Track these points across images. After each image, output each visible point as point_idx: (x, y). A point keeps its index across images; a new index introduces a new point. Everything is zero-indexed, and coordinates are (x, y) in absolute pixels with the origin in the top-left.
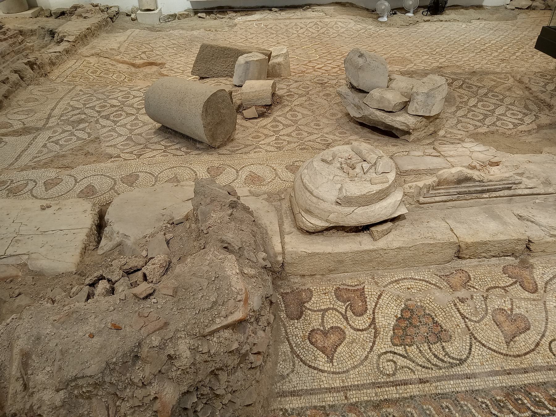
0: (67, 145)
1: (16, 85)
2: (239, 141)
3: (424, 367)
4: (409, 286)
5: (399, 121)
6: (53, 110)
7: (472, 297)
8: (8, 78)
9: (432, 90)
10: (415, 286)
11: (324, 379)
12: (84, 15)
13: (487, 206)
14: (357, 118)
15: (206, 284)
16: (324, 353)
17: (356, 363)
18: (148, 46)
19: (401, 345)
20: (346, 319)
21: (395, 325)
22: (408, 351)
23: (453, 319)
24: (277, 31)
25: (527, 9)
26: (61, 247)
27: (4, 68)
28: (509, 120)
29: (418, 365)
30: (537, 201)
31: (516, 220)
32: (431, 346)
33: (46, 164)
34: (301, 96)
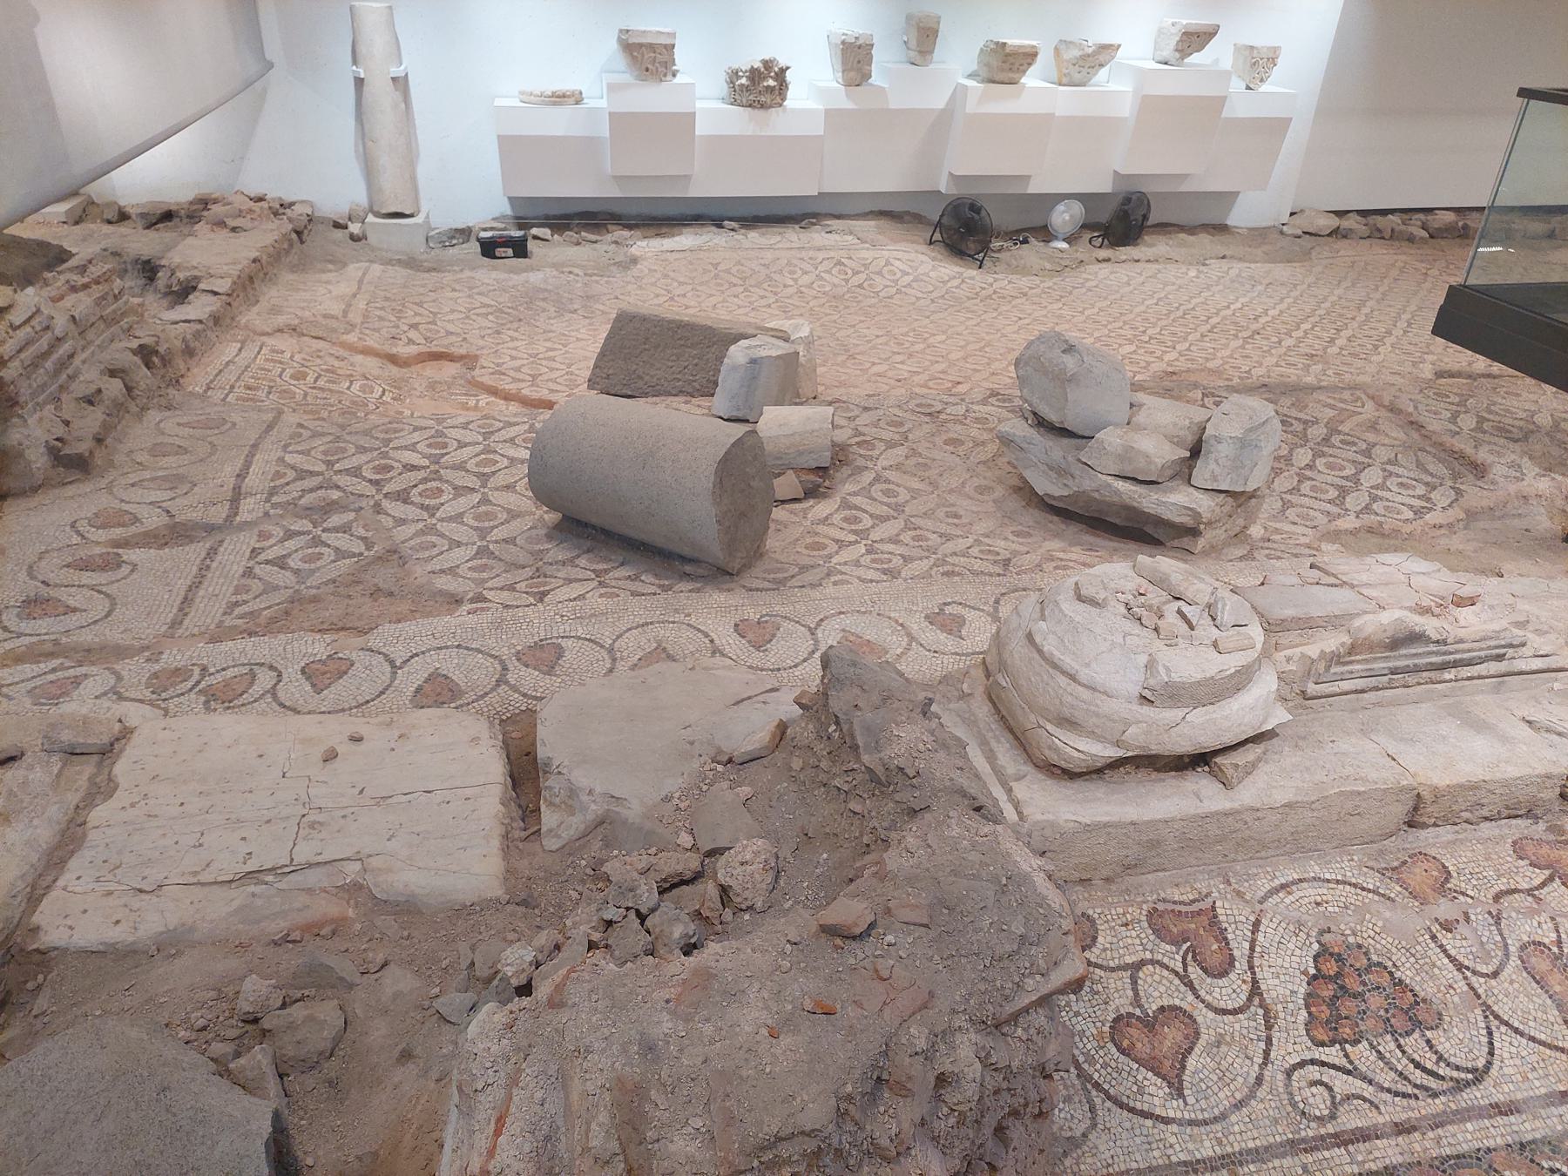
0: (313, 571)
1: (118, 408)
2: (776, 556)
3: (1397, 1094)
4: (1319, 899)
5: (1174, 502)
6: (241, 476)
7: (1467, 919)
8: (99, 391)
9: (1250, 430)
10: (1330, 898)
11: (1173, 1140)
12: (232, 223)
13: (1451, 701)
14: (1054, 498)
15: (991, 893)
16: (1157, 1074)
17: (1238, 1096)
18: (421, 310)
19: (1333, 1042)
20: (1190, 985)
21: (1308, 995)
22: (1352, 1057)
23: (1436, 971)
24: (716, 276)
25: (1330, 235)
26: (444, 837)
27: (84, 362)
28: (1399, 499)
29: (1382, 1089)
30: (1557, 686)
31: (1527, 731)
32: (1402, 1041)
33: (273, 620)
34: (891, 445)
